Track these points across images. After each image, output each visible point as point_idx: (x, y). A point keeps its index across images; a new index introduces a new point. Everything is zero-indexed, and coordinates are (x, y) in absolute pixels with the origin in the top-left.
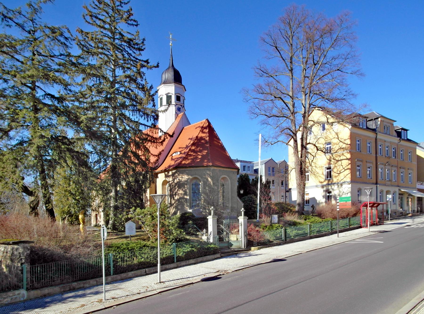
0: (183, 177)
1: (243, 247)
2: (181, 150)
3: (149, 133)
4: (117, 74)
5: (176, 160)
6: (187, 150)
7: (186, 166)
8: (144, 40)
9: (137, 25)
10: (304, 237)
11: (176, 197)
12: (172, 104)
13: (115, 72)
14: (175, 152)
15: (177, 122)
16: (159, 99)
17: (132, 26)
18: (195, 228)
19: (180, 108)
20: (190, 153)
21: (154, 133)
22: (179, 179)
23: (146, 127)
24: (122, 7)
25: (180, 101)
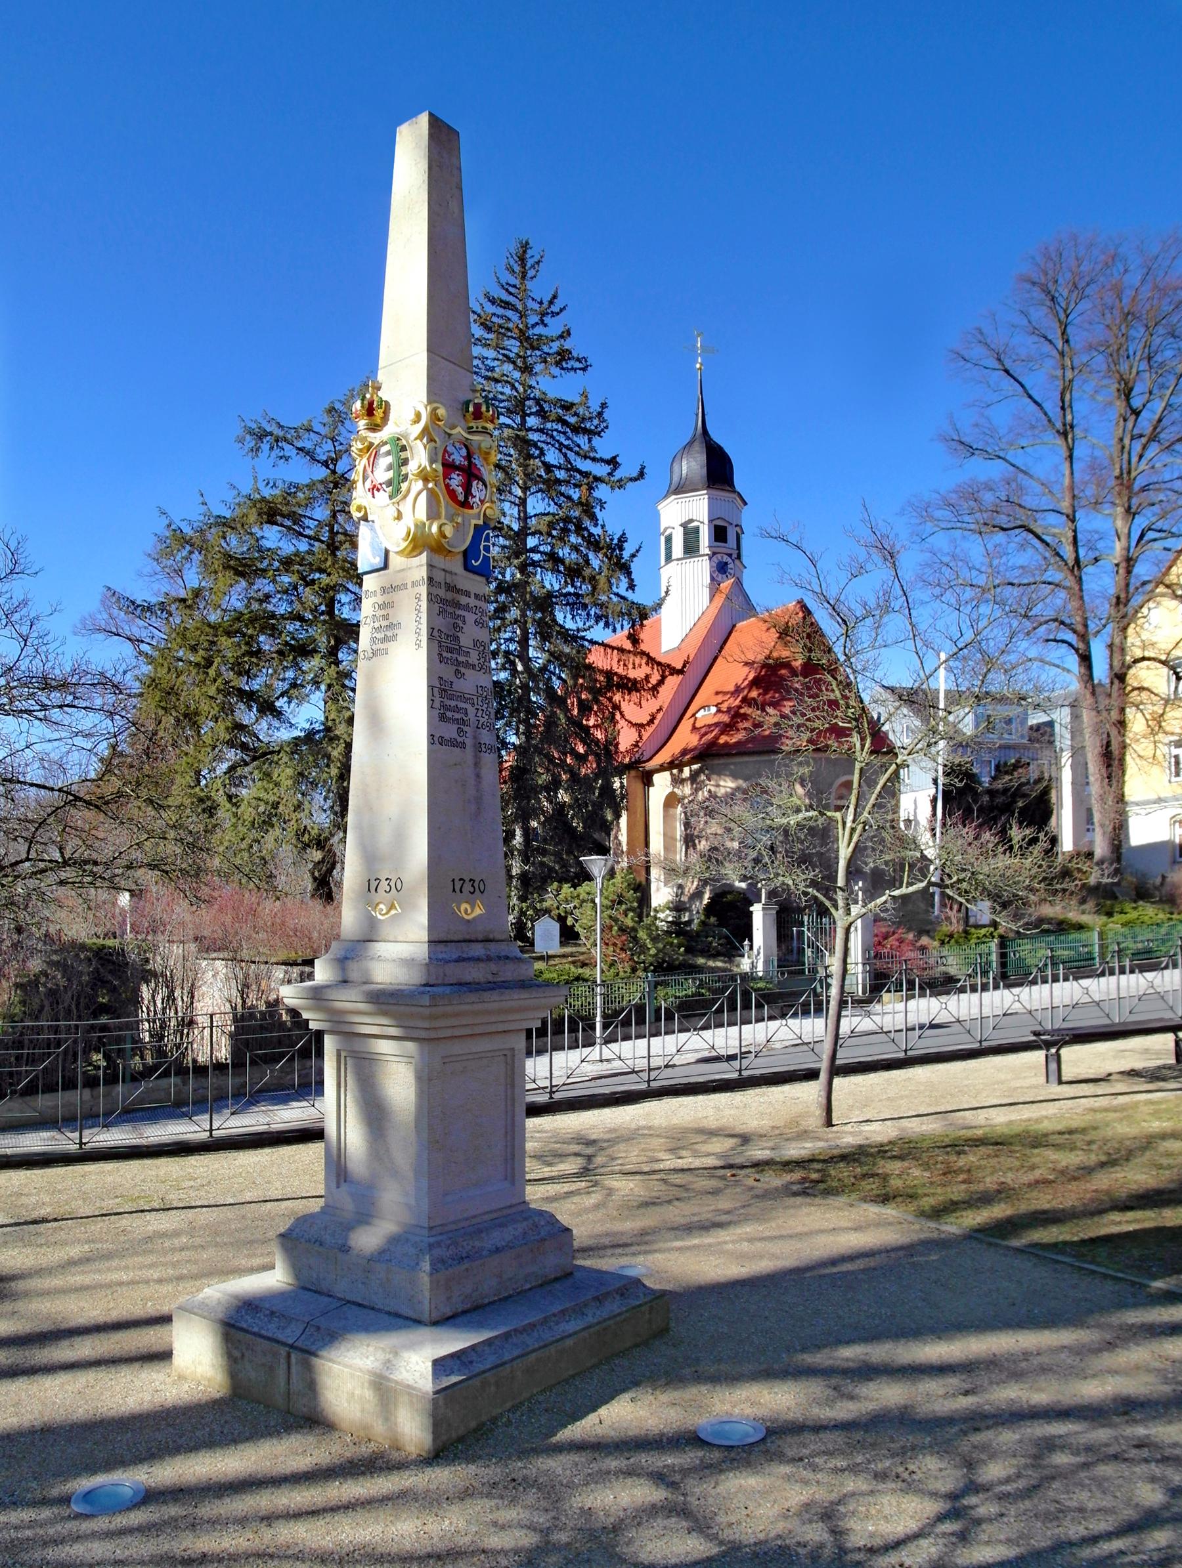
0: (722, 783)
1: (860, 993)
2: (720, 698)
3: (615, 669)
4: (531, 511)
5: (703, 731)
6: (737, 702)
7: (728, 752)
8: (604, 405)
9: (584, 369)
10: (1081, 968)
11: (703, 845)
12: (701, 552)
13: (525, 507)
14: (703, 707)
15: (714, 611)
16: (663, 539)
17: (572, 373)
18: (727, 937)
19: (726, 564)
20: (742, 711)
21: (630, 666)
22: (710, 791)
23: (609, 651)
24: (546, 325)
25: (725, 541)
